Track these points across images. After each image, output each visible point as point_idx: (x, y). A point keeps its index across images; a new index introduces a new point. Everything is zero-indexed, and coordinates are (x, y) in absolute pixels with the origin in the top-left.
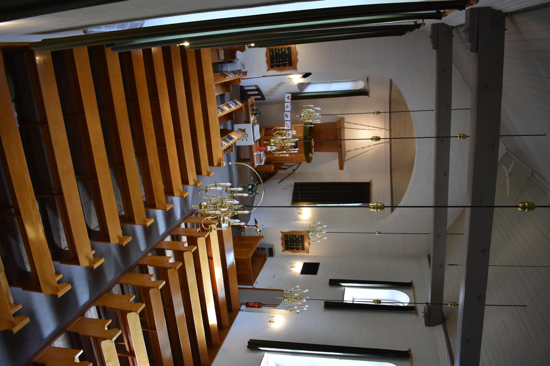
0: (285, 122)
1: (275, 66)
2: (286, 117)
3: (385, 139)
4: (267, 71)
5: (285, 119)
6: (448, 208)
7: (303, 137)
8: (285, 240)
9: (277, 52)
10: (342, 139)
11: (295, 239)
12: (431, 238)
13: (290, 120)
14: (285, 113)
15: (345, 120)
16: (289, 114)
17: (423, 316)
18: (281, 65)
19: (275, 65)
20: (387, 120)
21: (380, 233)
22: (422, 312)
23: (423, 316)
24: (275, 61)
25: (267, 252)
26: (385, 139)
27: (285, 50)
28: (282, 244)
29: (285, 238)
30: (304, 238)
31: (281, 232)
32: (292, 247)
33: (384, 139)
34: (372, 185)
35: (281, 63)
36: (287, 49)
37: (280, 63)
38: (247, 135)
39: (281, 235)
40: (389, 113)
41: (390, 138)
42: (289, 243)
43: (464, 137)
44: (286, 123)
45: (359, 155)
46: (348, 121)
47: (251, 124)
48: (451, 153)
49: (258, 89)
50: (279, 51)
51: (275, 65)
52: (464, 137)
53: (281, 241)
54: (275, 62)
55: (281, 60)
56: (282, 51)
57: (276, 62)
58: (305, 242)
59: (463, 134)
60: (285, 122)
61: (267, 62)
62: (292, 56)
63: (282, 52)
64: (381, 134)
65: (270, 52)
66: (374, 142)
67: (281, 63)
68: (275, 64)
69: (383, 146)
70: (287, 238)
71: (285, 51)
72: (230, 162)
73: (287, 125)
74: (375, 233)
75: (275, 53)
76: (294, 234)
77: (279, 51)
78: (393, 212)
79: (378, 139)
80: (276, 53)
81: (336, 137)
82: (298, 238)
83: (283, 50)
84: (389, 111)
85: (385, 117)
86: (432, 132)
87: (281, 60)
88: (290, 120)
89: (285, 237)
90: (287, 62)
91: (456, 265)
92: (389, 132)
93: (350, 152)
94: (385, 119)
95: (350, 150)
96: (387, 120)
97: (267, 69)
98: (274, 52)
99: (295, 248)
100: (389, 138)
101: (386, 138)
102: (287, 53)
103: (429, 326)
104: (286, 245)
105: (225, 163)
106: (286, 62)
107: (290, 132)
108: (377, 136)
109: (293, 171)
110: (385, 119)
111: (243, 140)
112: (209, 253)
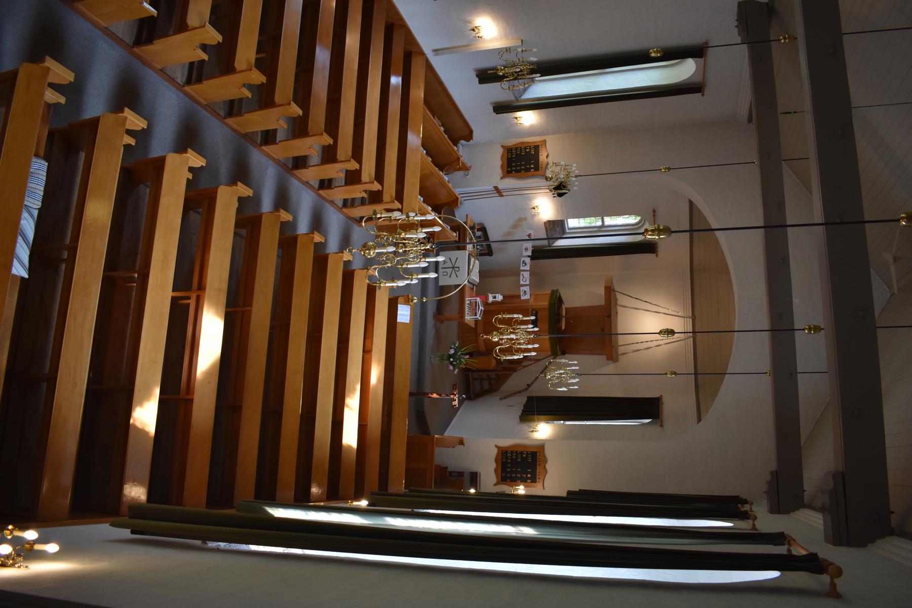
0: (522, 273)
1: (514, 172)
2: (524, 265)
3: (685, 333)
4: (501, 178)
5: (522, 268)
6: (796, 331)
7: (547, 307)
8: (502, 462)
9: (514, 457)
10: (613, 333)
11: (524, 153)
12: (766, 382)
13: (528, 269)
14: (522, 288)
15: (619, 303)
16: (527, 289)
17: (736, 27)
18: (523, 169)
19: (514, 170)
20: (688, 306)
21: (675, 373)
22: (735, 25)
23: (736, 27)
24: (509, 470)
25: (467, 478)
26: (685, 333)
27: (530, 150)
28: (496, 470)
29: (502, 458)
30: (539, 151)
31: (496, 446)
32: (514, 475)
33: (683, 334)
34: (663, 404)
35: (519, 475)
36: (530, 456)
37: (516, 475)
38: (459, 267)
39: (495, 451)
40: (693, 375)
41: (694, 332)
42: (509, 467)
43: (817, 329)
44: (523, 275)
45: (641, 343)
46: (624, 304)
47: (467, 253)
48: (796, 301)
49: (483, 229)
50: (521, 151)
51: (514, 170)
52: (817, 329)
53: (494, 465)
54: (514, 166)
55: (520, 470)
56: (521, 456)
57: (515, 166)
58: (539, 465)
59: (813, 325)
60: (522, 273)
61: (502, 167)
62: (540, 157)
63: (526, 152)
64: (677, 324)
65: (508, 153)
66: (664, 339)
67: (519, 475)
68: (513, 169)
69: (680, 346)
70: (507, 458)
71: (530, 151)
72: (424, 298)
73: (524, 277)
74: (666, 374)
75: (510, 458)
76: (519, 450)
77: (521, 151)
78: (700, 423)
79: (670, 332)
80: (512, 458)
81: (603, 330)
82: (527, 457)
83: (528, 150)
84: (691, 331)
85: (685, 304)
86: (764, 322)
87: (520, 470)
88: (528, 269)
89: (502, 455)
90: (529, 476)
91: (795, 112)
92: (691, 319)
93: (625, 356)
94: (685, 301)
95: (625, 352)
96: (688, 306)
97: (502, 176)
98: (509, 456)
99: (519, 478)
100: (691, 331)
101: (686, 331)
102: (530, 461)
103: (779, 513)
104: (508, 167)
105: (416, 299)
106: (527, 475)
107: (529, 350)
108: (669, 328)
109: (527, 387)
110: (685, 301)
111: (450, 277)
112: (368, 344)
